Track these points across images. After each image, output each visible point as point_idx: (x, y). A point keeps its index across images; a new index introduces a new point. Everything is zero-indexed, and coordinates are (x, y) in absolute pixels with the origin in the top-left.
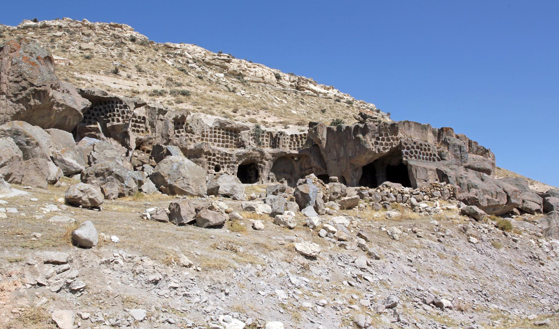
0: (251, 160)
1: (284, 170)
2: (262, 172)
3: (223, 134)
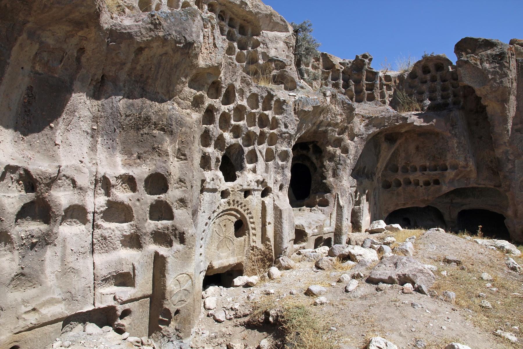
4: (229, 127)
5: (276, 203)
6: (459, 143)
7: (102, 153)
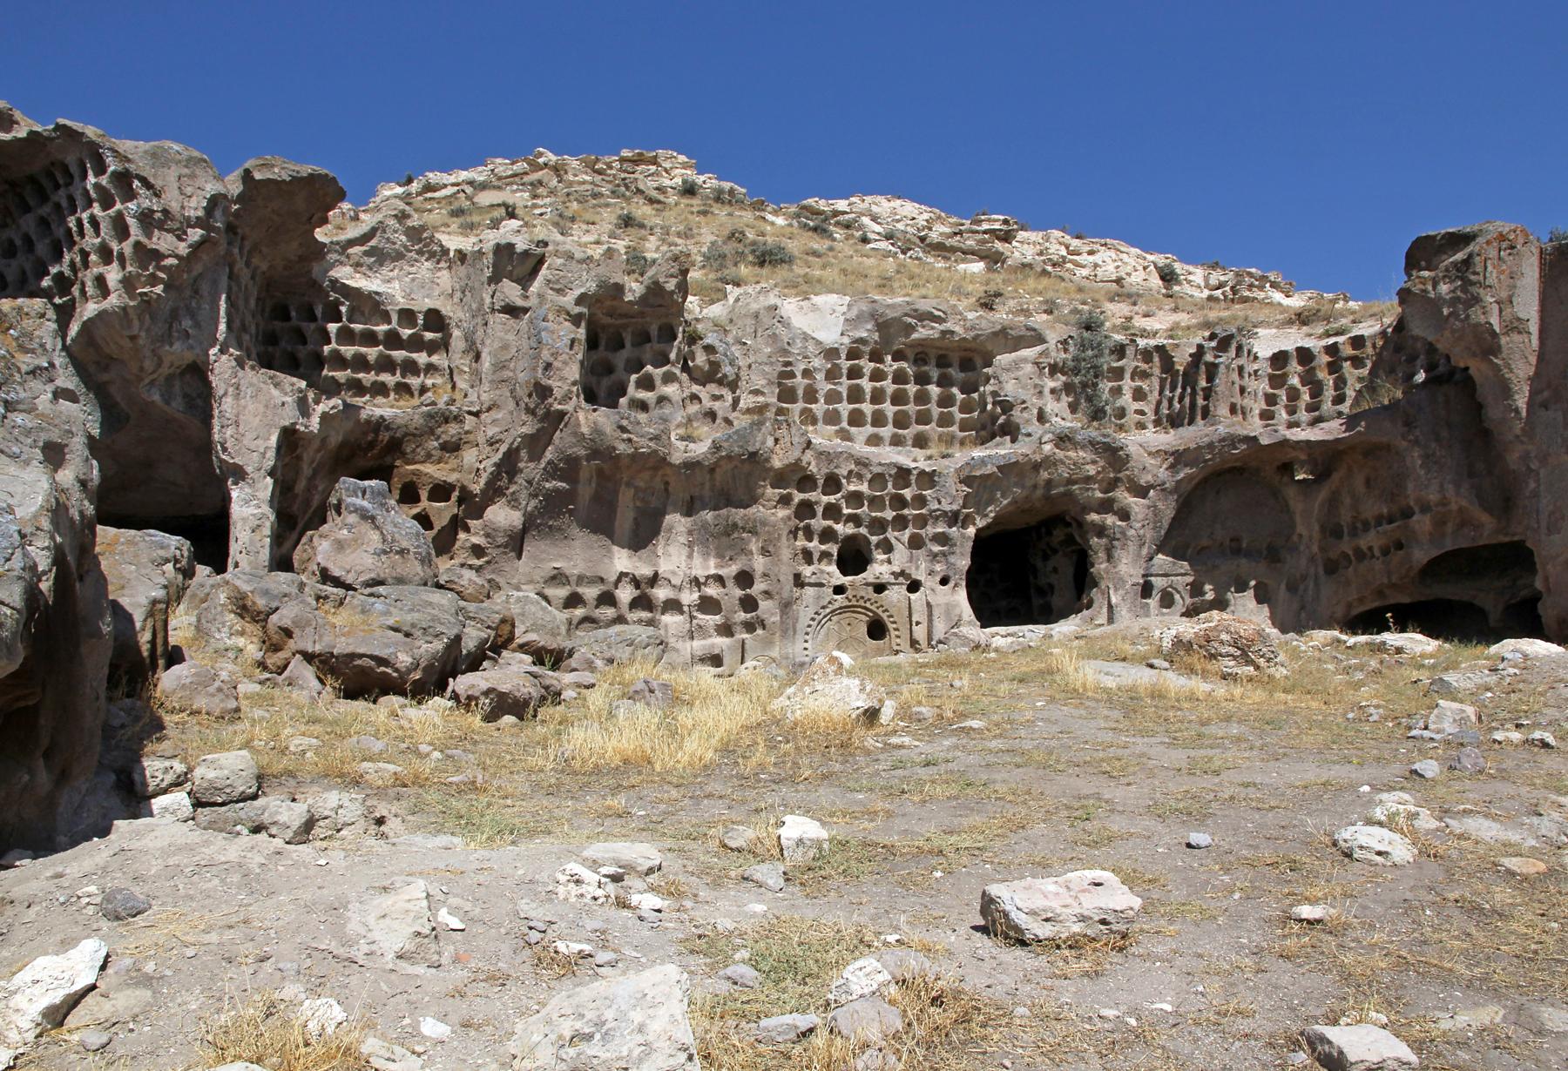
0: (1047, 498)
1: (1236, 539)
2: (1110, 557)
3: (899, 378)
6: (1426, 457)
7: (697, 560)
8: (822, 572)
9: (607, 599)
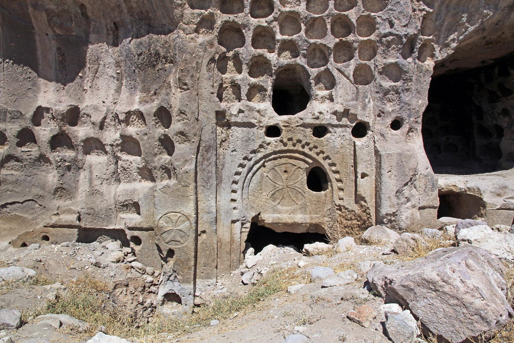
4: (275, 44)
5: (376, 145)
8: (251, 109)
9: (26, 137)
